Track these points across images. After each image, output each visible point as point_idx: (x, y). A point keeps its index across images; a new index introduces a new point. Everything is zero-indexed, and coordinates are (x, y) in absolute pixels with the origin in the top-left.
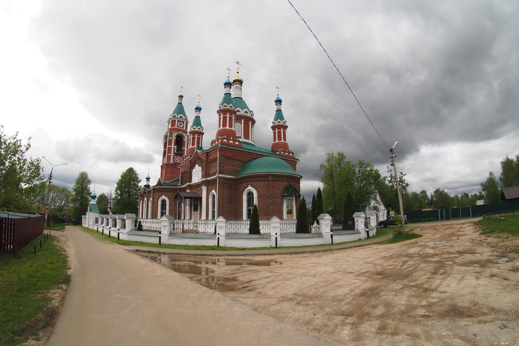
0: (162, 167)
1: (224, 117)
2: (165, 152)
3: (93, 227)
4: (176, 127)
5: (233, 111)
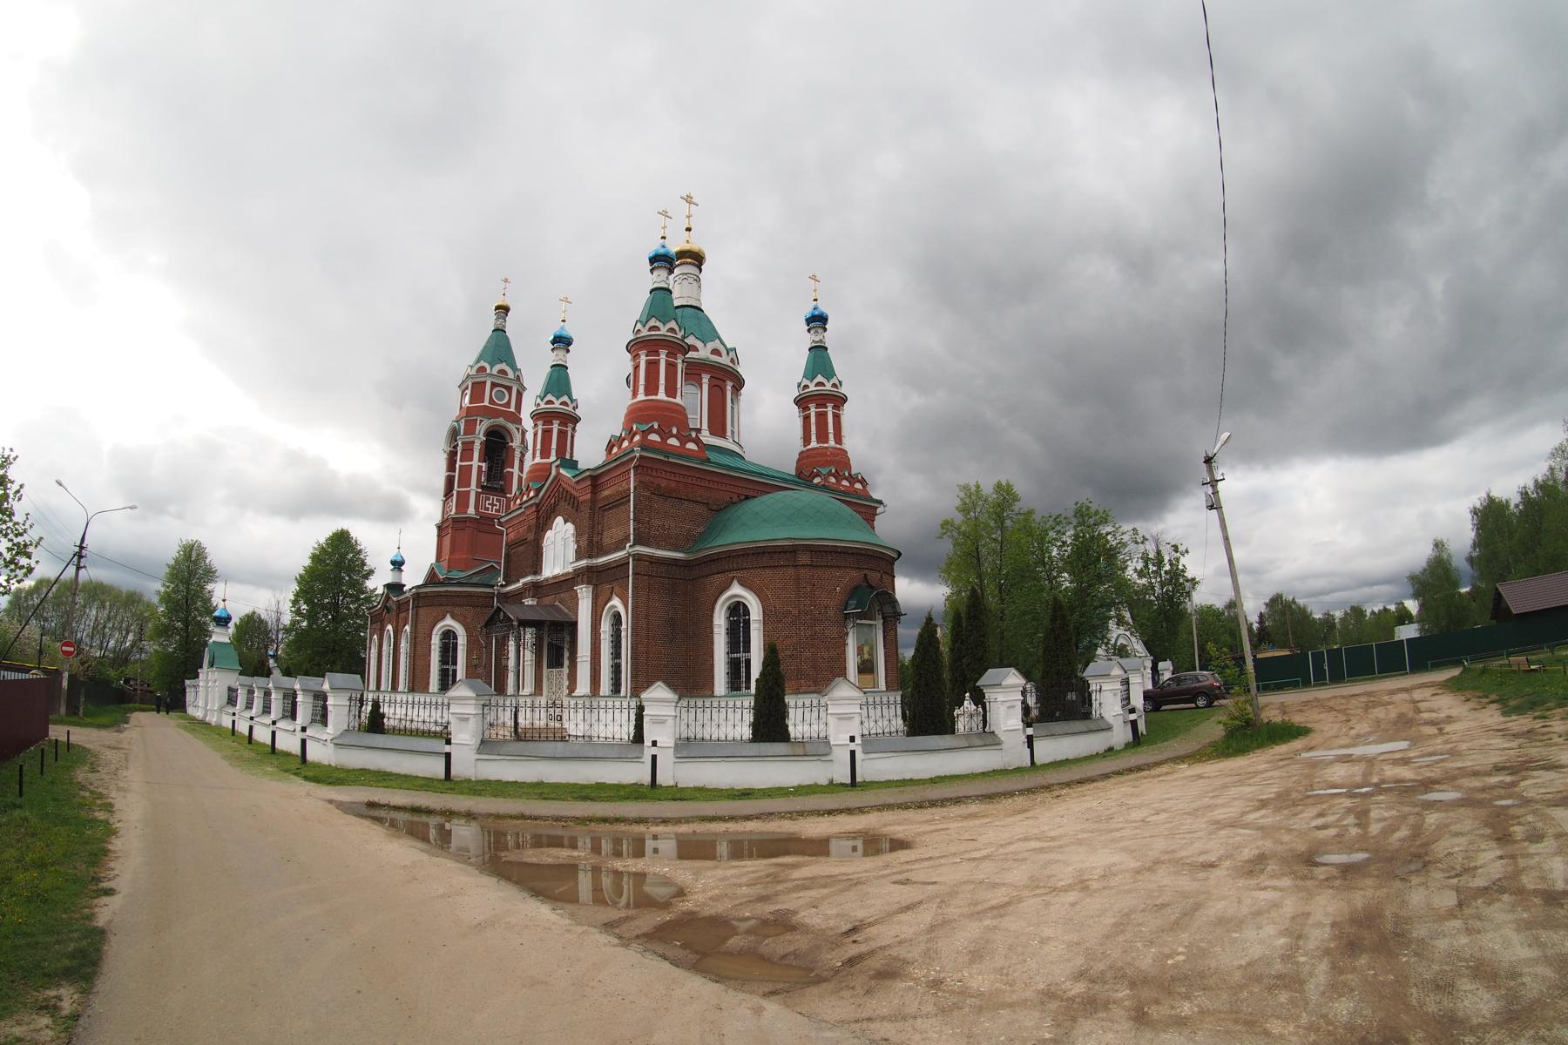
0: (440, 528)
1: (649, 363)
2: (450, 482)
3: (219, 718)
4: (486, 403)
5: (676, 347)
